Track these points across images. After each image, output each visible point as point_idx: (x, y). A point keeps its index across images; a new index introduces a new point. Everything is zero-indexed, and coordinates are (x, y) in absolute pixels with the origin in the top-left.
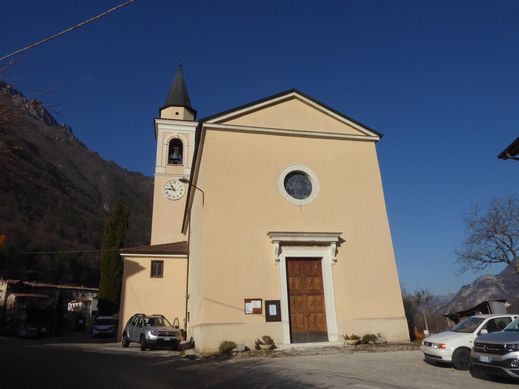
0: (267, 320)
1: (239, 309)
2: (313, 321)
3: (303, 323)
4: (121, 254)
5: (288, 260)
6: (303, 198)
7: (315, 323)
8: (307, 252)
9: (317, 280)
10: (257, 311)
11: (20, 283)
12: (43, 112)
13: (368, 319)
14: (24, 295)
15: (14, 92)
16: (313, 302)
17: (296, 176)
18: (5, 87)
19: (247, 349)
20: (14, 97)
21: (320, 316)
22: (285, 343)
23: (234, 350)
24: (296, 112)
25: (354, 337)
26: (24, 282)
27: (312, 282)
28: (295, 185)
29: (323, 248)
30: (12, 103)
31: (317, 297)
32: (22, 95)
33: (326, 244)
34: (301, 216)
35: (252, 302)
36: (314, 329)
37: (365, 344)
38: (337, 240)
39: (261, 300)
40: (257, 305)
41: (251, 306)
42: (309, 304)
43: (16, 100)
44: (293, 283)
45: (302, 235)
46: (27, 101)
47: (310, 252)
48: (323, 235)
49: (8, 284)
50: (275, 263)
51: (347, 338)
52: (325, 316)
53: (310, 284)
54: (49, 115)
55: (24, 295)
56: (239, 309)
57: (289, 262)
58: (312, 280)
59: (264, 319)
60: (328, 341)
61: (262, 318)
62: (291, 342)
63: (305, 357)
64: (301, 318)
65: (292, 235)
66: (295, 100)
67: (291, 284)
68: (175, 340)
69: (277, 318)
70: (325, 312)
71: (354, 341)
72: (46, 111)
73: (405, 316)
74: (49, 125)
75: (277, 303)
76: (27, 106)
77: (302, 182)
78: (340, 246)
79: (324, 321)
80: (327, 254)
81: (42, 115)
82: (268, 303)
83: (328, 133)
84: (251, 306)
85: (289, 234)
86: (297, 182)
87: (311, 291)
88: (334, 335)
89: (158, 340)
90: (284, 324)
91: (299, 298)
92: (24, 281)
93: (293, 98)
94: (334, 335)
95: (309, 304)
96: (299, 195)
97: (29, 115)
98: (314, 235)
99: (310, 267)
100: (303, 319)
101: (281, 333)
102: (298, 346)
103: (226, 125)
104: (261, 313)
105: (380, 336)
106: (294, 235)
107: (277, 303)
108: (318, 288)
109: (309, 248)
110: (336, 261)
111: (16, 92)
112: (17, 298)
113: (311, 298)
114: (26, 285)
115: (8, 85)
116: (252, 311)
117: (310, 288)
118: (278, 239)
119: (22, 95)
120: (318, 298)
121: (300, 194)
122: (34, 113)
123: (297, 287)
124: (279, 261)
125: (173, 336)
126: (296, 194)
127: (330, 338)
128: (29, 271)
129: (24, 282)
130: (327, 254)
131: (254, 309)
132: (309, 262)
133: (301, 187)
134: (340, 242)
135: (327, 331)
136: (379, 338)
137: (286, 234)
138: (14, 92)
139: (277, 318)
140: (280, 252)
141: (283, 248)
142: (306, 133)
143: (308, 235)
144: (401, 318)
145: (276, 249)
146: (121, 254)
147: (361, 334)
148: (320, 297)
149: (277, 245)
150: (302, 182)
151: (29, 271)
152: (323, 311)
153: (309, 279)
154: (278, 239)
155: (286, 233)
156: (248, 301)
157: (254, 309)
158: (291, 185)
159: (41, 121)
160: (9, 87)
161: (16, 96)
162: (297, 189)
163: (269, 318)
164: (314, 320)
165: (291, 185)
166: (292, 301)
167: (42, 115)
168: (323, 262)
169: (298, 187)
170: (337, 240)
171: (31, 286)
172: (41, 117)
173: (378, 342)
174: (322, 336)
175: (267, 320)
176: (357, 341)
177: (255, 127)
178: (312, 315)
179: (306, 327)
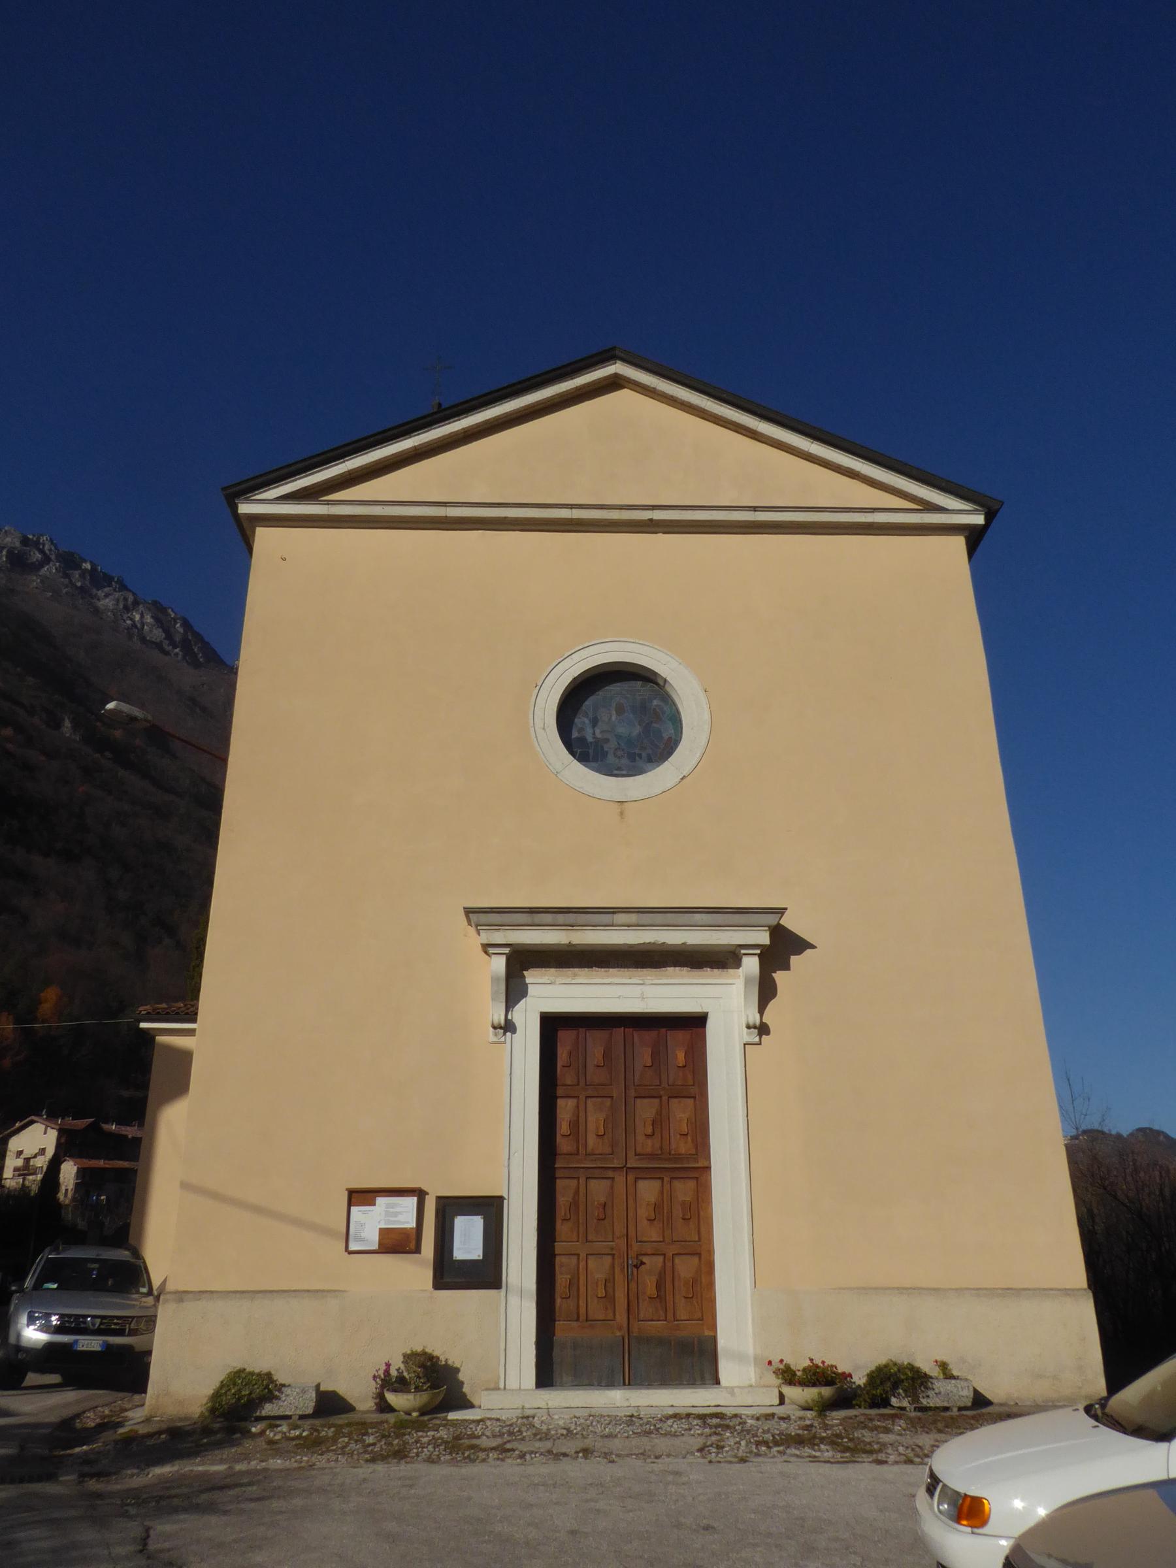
0: (440, 1282)
1: (327, 1232)
2: (651, 1290)
3: (609, 1299)
4: (143, 1025)
5: (553, 1026)
6: (641, 772)
7: (660, 1296)
8: (637, 990)
9: (681, 1112)
10: (396, 1243)
11: (94, 1127)
12: (181, 630)
13: (902, 1290)
14: (101, 1163)
15: (99, 579)
16: (657, 1207)
17: (614, 690)
18: (77, 566)
19: (330, 1405)
20: (100, 593)
21: (685, 1268)
22: (512, 1383)
23: (268, 1409)
24: (633, 435)
25: (818, 1376)
26: (105, 1127)
27: (660, 1122)
28: (607, 716)
29: (709, 976)
30: (97, 611)
31: (677, 1184)
32: (123, 587)
33: (721, 959)
34: (618, 845)
35: (381, 1201)
36: (656, 1327)
37: (874, 1405)
38: (764, 938)
39: (420, 1194)
40: (403, 1213)
41: (371, 1221)
42: (643, 1212)
43: (107, 602)
44: (575, 1125)
45: (606, 918)
46: (136, 603)
47: (650, 991)
48: (698, 918)
49: (61, 1132)
50: (492, 1038)
51: (788, 1376)
52: (708, 1268)
53: (649, 1131)
54: (196, 635)
55: (101, 1163)
56: (327, 1232)
57: (566, 1040)
58: (659, 1113)
59: (427, 1275)
60: (718, 1382)
61: (417, 1271)
62: (545, 1379)
63: (511, 1468)
64: (600, 1276)
65: (561, 918)
66: (625, 394)
67: (563, 1127)
68: (128, 1348)
69: (486, 1274)
70: (710, 1252)
71: (810, 1394)
72: (186, 624)
73: (1085, 1284)
74: (196, 665)
75: (490, 1209)
76: (137, 617)
77: (643, 709)
78: (787, 967)
79: (701, 1290)
80: (724, 1000)
81: (178, 638)
82: (450, 1208)
83: (755, 509)
84: (371, 1221)
85: (548, 918)
86: (620, 710)
87: (652, 1156)
88: (740, 1358)
89: (49, 1346)
90: (514, 1300)
91: (598, 1189)
92: (106, 1123)
93: (614, 384)
94: (740, 1358)
95: (643, 1212)
96: (625, 761)
97: (143, 640)
98: (670, 918)
99: (654, 1055)
100: (609, 1282)
101: (496, 1341)
102: (569, 1402)
103: (328, 503)
104: (418, 1250)
105: (949, 1376)
106: (571, 918)
107: (490, 1209)
108: (684, 1147)
109: (649, 975)
110: (763, 1029)
111: (107, 580)
112: (82, 1173)
113: (648, 1190)
114: (111, 1135)
115: (85, 561)
116: (373, 1241)
117: (649, 1146)
118: (499, 937)
119: (123, 587)
120: (683, 1190)
121: (632, 757)
122: (158, 634)
123: (591, 1141)
124: (508, 1027)
125: (120, 1333)
126: (611, 759)
127: (727, 1371)
128: (126, 1094)
129: (105, 1127)
130: (724, 1001)
131: (384, 1232)
132: (650, 1035)
133: (636, 730)
134: (782, 947)
135: (714, 1340)
136: (941, 1386)
137: (534, 914)
138: (99, 579)
139: (486, 1274)
140: (514, 991)
141: (534, 978)
142: (658, 515)
143: (633, 918)
144: (1067, 1292)
145: (495, 980)
146: (143, 1025)
147: (857, 1362)
148: (691, 1184)
149: (499, 964)
150: (643, 709)
151: (126, 1094)
152: (700, 1251)
153: (646, 1110)
154: (499, 937)
155: (533, 911)
156: (360, 1196)
157: (384, 1232)
158: (595, 722)
159: (176, 654)
160: (88, 566)
161: (107, 589)
162: (619, 737)
163: (450, 1274)
164: (659, 1286)
165: (595, 722)
166: (563, 1200)
167: (178, 638)
168: (713, 1031)
169: (622, 730)
170: (764, 938)
171: (126, 1136)
172: (175, 647)
173: (932, 1401)
174: (696, 1358)
175: (440, 1282)
176: (827, 1391)
177: (444, 504)
178: (653, 1263)
179: (621, 1317)
